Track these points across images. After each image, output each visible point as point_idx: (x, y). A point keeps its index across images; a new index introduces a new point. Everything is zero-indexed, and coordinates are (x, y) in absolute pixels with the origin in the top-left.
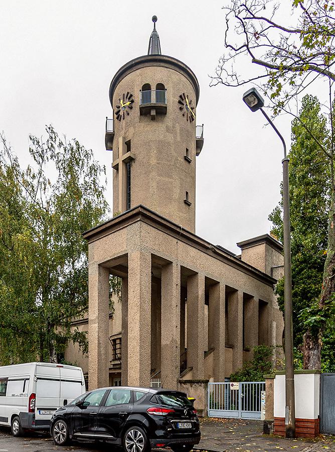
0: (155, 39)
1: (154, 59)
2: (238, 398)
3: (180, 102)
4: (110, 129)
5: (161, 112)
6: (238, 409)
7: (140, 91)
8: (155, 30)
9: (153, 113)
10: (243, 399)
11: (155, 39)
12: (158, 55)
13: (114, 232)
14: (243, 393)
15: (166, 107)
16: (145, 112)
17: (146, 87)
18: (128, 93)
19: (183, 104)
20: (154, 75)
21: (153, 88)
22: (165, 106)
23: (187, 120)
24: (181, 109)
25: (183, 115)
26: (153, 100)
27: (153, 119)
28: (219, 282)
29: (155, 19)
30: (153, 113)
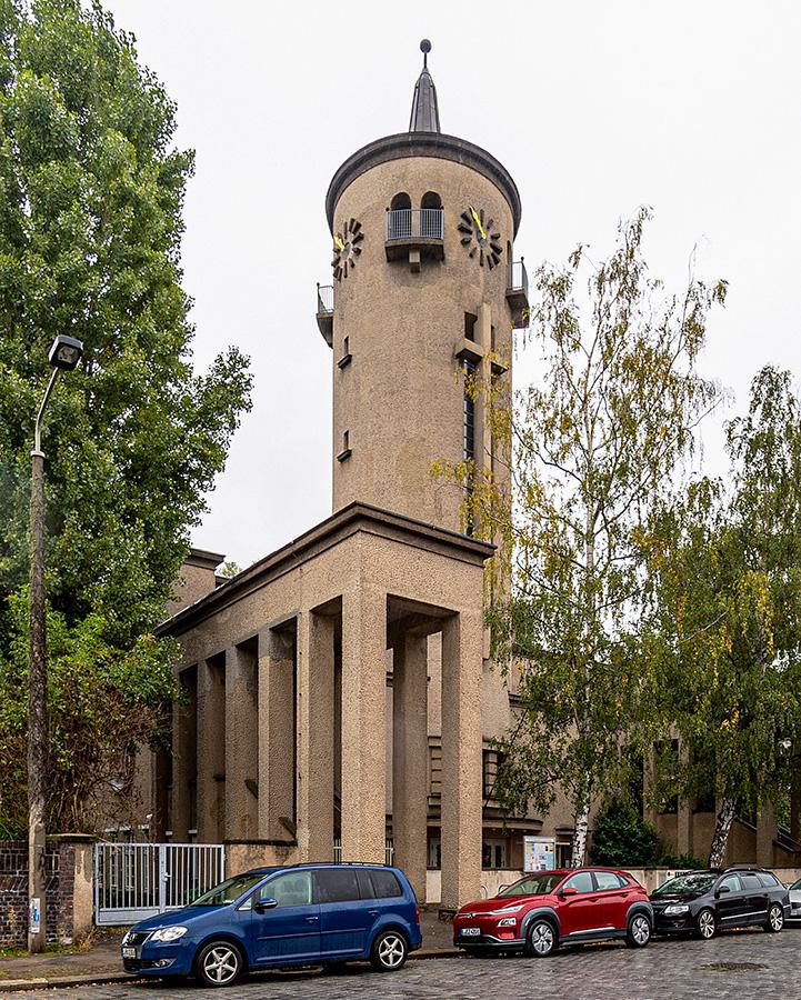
0: (425, 92)
1: (424, 141)
2: (157, 885)
3: (462, 229)
4: (329, 305)
5: (433, 255)
6: (157, 904)
7: (387, 210)
8: (425, 71)
9: (415, 258)
10: (168, 883)
11: (425, 92)
12: (431, 134)
13: (263, 586)
14: (168, 871)
15: (442, 246)
16: (397, 255)
17: (401, 202)
18: (353, 220)
19: (471, 233)
20: (419, 172)
21: (416, 204)
22: (438, 243)
23: (482, 265)
24: (465, 243)
25: (471, 256)
26: (416, 231)
27: (415, 270)
28: (457, 613)
29: (426, 47)
30: (415, 258)
